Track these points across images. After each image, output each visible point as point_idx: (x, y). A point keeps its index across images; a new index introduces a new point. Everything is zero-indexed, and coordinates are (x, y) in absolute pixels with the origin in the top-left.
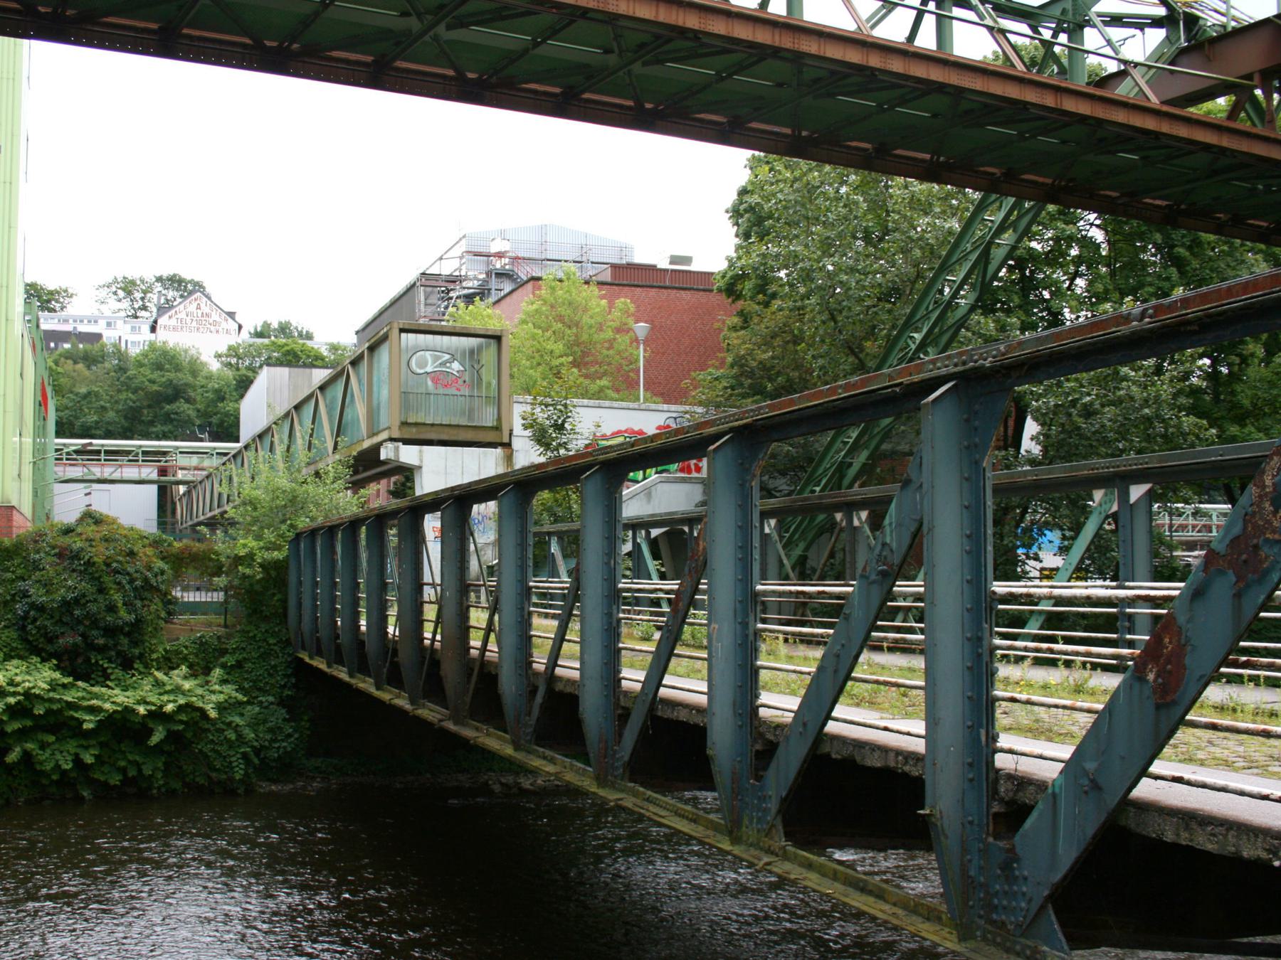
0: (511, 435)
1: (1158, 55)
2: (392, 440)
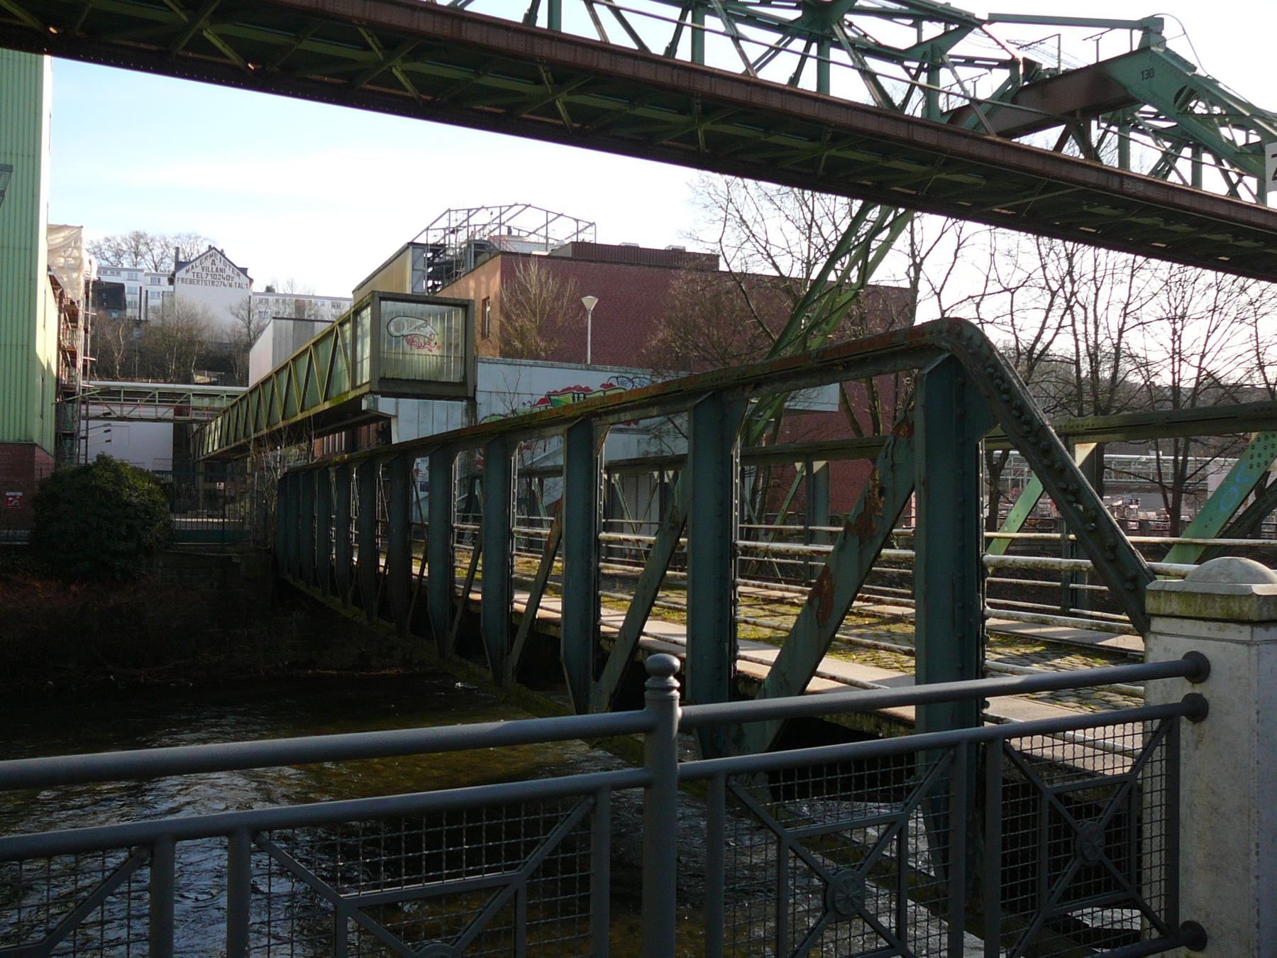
0: (475, 390)
1: (1001, 94)
2: (371, 392)
